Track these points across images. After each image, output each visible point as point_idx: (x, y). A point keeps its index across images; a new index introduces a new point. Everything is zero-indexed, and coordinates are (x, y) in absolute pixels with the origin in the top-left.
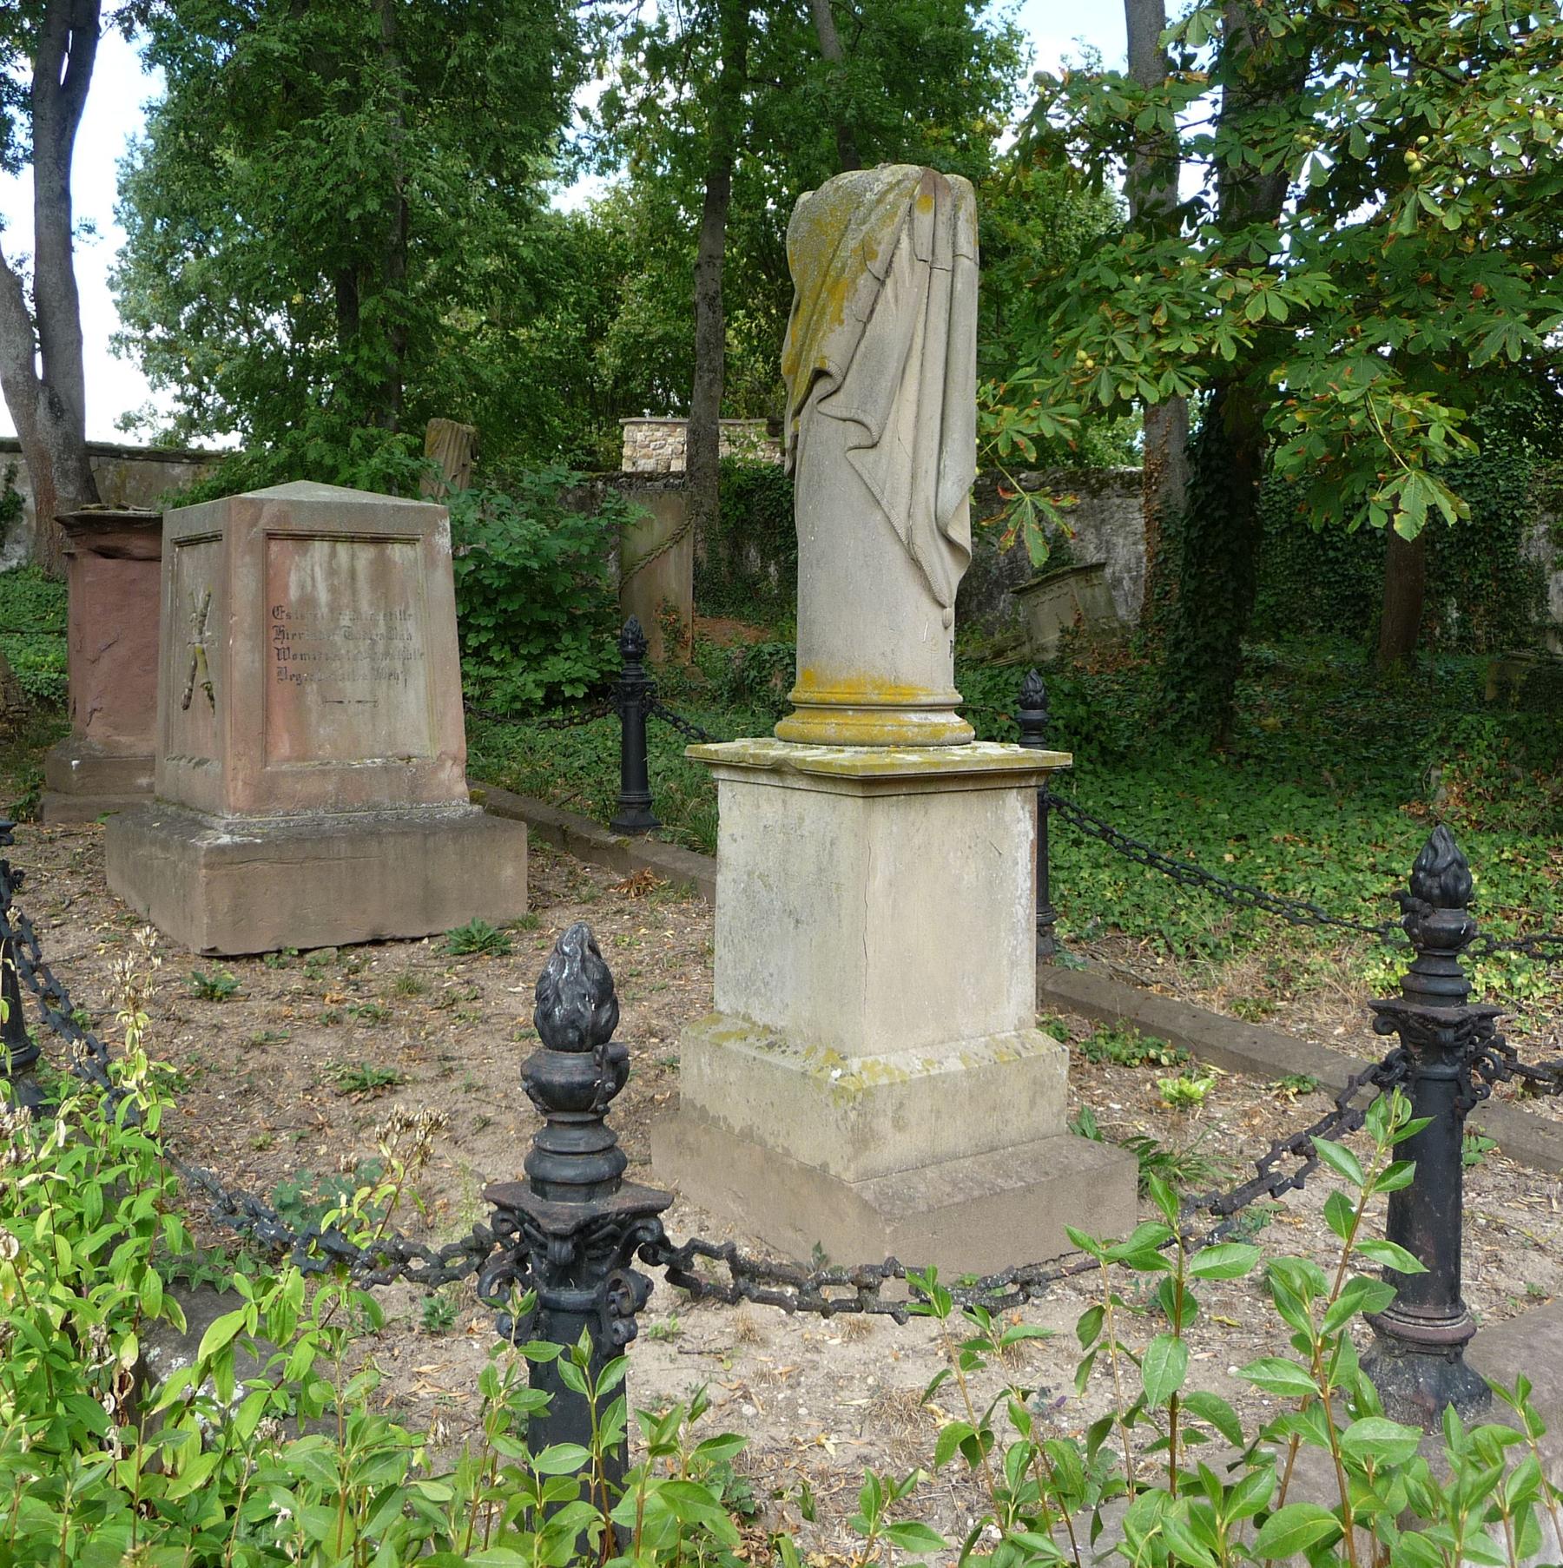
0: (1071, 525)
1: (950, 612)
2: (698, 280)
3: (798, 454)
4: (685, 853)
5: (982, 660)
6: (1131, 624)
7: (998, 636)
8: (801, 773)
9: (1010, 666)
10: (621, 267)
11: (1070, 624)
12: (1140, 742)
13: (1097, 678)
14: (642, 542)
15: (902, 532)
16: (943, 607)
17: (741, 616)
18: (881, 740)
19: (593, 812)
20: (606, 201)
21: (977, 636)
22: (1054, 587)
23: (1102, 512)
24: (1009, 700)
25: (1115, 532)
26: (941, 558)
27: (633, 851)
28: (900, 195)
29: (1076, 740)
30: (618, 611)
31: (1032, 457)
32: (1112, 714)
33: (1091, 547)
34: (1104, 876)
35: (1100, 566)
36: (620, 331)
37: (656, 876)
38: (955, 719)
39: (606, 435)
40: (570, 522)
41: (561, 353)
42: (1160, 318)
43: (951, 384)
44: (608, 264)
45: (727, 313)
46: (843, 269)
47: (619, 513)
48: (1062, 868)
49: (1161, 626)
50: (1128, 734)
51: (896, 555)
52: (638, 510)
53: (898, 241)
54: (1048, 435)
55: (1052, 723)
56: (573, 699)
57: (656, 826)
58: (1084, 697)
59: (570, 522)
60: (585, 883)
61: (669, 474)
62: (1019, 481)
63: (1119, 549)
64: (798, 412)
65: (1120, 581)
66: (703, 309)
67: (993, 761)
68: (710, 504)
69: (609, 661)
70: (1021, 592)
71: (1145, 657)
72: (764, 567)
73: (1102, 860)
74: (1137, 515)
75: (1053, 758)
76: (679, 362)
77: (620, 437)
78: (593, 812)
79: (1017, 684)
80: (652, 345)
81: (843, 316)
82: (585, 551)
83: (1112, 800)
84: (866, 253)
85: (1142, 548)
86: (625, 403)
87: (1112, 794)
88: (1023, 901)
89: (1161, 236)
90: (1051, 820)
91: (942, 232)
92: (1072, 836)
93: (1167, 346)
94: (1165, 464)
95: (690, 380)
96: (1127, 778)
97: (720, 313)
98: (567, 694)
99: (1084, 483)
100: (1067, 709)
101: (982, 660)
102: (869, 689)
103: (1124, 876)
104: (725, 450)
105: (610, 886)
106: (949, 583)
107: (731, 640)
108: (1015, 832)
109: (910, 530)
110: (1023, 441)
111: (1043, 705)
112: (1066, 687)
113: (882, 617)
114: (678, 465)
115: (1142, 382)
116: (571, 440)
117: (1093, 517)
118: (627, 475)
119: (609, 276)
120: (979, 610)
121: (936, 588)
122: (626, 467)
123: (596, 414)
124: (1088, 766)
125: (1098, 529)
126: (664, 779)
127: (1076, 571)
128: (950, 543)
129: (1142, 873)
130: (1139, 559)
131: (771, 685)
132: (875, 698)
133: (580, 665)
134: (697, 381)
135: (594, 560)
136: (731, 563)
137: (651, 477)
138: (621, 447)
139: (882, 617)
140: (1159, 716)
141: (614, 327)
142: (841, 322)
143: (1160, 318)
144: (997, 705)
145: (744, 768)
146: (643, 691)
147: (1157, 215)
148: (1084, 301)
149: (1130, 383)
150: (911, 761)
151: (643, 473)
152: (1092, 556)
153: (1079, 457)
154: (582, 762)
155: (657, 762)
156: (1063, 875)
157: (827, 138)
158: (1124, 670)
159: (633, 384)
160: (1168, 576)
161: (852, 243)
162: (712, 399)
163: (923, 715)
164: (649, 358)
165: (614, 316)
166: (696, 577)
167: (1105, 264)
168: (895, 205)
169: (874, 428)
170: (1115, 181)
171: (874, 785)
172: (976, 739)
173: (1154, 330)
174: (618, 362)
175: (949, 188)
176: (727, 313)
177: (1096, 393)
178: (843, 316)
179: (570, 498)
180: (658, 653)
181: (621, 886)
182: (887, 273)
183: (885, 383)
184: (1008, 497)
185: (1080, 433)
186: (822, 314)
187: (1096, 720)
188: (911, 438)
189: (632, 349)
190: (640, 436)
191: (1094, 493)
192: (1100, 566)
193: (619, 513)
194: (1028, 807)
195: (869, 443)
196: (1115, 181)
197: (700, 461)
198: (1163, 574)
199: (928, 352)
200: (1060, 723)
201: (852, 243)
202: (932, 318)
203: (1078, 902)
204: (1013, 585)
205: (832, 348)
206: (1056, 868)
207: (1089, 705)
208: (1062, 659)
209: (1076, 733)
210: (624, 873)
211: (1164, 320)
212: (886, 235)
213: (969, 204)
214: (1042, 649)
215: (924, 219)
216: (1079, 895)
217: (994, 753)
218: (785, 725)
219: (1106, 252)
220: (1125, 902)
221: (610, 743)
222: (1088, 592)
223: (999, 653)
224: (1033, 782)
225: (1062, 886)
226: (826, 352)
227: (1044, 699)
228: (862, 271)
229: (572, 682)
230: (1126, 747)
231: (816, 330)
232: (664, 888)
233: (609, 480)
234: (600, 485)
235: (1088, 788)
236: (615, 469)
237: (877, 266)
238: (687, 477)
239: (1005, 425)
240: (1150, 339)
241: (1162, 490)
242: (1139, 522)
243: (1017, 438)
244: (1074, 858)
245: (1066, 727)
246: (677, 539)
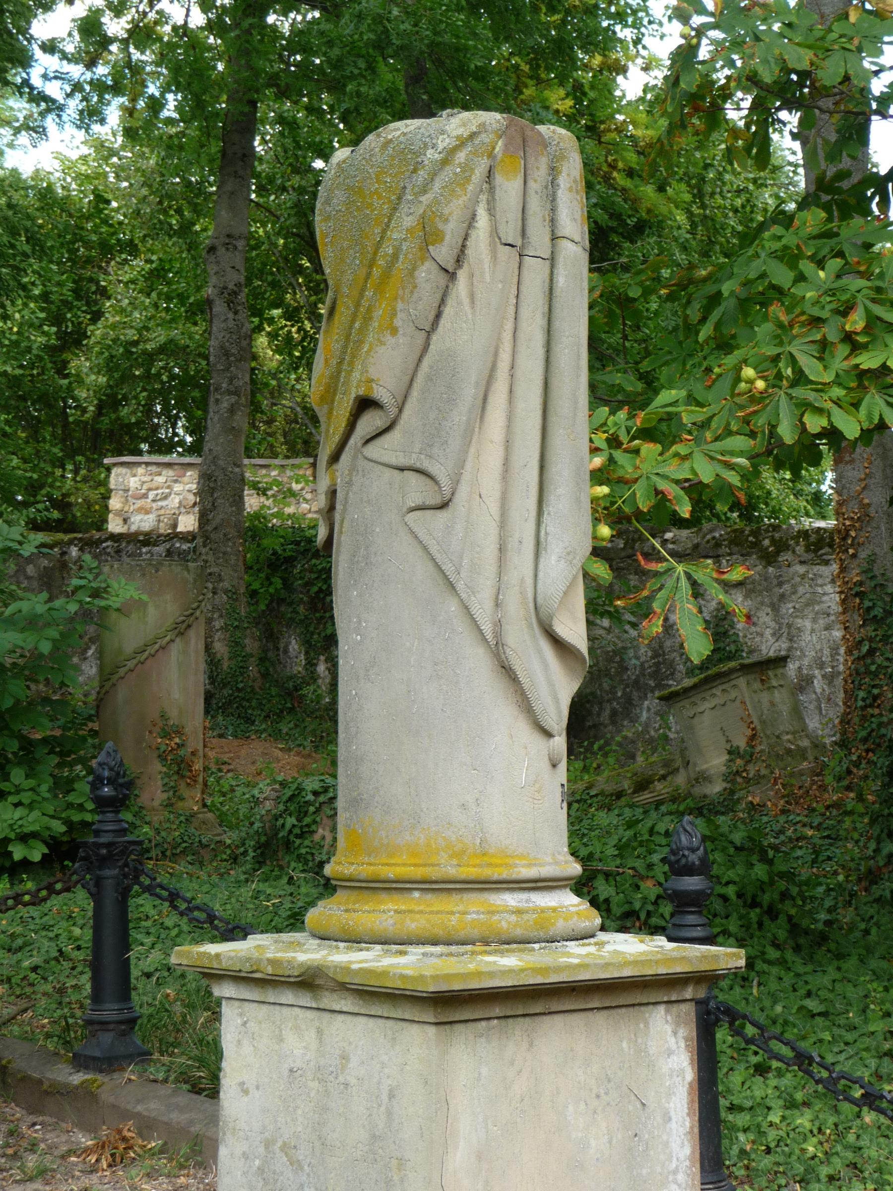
0: (738, 603)
1: (560, 742)
2: (212, 269)
3: (337, 517)
4: (185, 1098)
5: (619, 795)
6: (827, 741)
7: (640, 759)
8: (343, 987)
9: (658, 804)
10: (106, 249)
11: (741, 743)
12: (847, 916)
13: (782, 819)
14: (129, 634)
15: (487, 628)
16: (548, 734)
17: (277, 735)
18: (462, 934)
19: (48, 1036)
20: (84, 158)
21: (611, 760)
22: (717, 691)
23: (780, 584)
24: (656, 858)
25: (799, 612)
26: (546, 666)
27: (106, 1096)
28: (475, 153)
29: (754, 914)
30: (94, 733)
31: (685, 510)
32: (805, 873)
33: (768, 632)
34: (803, 1121)
35: (780, 661)
36: (104, 336)
37: (140, 1135)
38: (569, 900)
39: (85, 480)
40: (25, 606)
41: (21, 366)
42: (856, 322)
43: (552, 419)
44: (88, 245)
45: (257, 312)
46: (395, 256)
47: (96, 594)
48: (741, 1109)
49: (870, 745)
50: (828, 903)
51: (477, 663)
52: (123, 588)
53: (473, 217)
54: (706, 481)
55: (719, 890)
56: (25, 864)
57: (142, 1056)
58: (763, 853)
59: (25, 606)
60: (33, 1147)
61: (175, 536)
62: (664, 542)
63: (806, 637)
64: (335, 458)
65: (809, 680)
66: (219, 307)
67: (627, 963)
68: (232, 578)
69: (81, 807)
70: (670, 698)
71: (848, 788)
72: (311, 664)
73: (799, 1096)
74: (829, 588)
75: (716, 957)
76: (187, 381)
77: (105, 483)
78: (48, 1036)
79: (667, 834)
80: (150, 357)
81: (398, 322)
82: (45, 648)
83: (812, 1005)
84: (428, 234)
85: (838, 634)
86: (118, 435)
87: (809, 994)
88: (681, 1177)
89: (846, 214)
90: (722, 1035)
91: (536, 205)
92: (754, 1060)
93: (868, 361)
94: (865, 518)
95: (203, 404)
96: (831, 969)
97: (243, 314)
98: (17, 856)
99: (754, 545)
100: (740, 869)
101: (619, 795)
102: (443, 858)
103: (831, 1120)
104: (252, 502)
105: (70, 1153)
106: (556, 700)
107: (259, 770)
108: (665, 1070)
109: (498, 624)
110: (673, 490)
111: (703, 868)
112: (738, 837)
113: (461, 751)
114: (188, 523)
115: (835, 410)
116: (33, 488)
117: (769, 592)
118: (116, 538)
119: (89, 261)
120: (613, 722)
121: (538, 708)
122: (114, 526)
123: (71, 453)
124: (773, 954)
125: (775, 608)
126: (158, 984)
127: (746, 669)
128: (557, 642)
129: (858, 1116)
130: (835, 650)
131: (317, 837)
132: (452, 871)
133: (36, 814)
134: (212, 407)
135: (60, 654)
136: (262, 660)
137: (147, 539)
138: (106, 497)
139: (461, 751)
140: (872, 877)
141: (97, 332)
142: (394, 331)
143: (856, 322)
144: (639, 864)
145: (261, 981)
146: (125, 852)
147: (839, 191)
148: (744, 304)
149: (820, 411)
150: (507, 966)
151: (137, 533)
152: (770, 647)
153: (747, 510)
154: (36, 960)
155: (144, 958)
156: (742, 1119)
157: (391, 74)
158: (820, 808)
159: (124, 411)
160: (875, 674)
161: (407, 220)
162: (234, 431)
163: (524, 896)
164: (147, 376)
165: (97, 316)
166: (212, 679)
167: (773, 254)
168: (467, 168)
169: (444, 481)
170: (786, 146)
171: (452, 1006)
172: (603, 928)
173: (848, 338)
174: (102, 380)
175: (544, 143)
176: (257, 312)
177: (773, 427)
178: (398, 322)
179: (30, 570)
180: (153, 793)
181: (87, 1151)
182: (459, 261)
183: (460, 416)
184: (654, 566)
185: (750, 476)
186: (368, 319)
187: (782, 885)
188: (497, 494)
189: (125, 363)
190: (133, 483)
191: (769, 559)
192: (780, 661)
193: (96, 594)
194: (682, 1032)
195: (437, 501)
196: (786, 146)
197: (217, 518)
198: (868, 672)
199: (519, 373)
200: (731, 891)
201: (407, 220)
202: (523, 324)
203: (767, 1162)
204: (659, 686)
205: (382, 366)
206: (732, 1108)
207: (770, 862)
208: (732, 792)
209: (754, 904)
210: (90, 1129)
211: (860, 325)
212: (455, 209)
213: (572, 169)
214: (703, 778)
215: (509, 188)
216: (768, 1151)
217: (630, 951)
218: (323, 913)
219: (769, 241)
220: (835, 1160)
221: (77, 931)
222: (765, 697)
223: (642, 785)
224: (689, 993)
225: (742, 1137)
226: (373, 373)
227: (704, 860)
228: (423, 260)
229: (24, 838)
230: (828, 923)
231: (360, 343)
232: (152, 1153)
233: (87, 545)
234: (74, 551)
235: (773, 986)
236: (99, 529)
237: (444, 253)
238: (199, 541)
239: (645, 468)
240: (843, 350)
241: (863, 554)
242: (831, 598)
243: (663, 485)
244: (758, 1093)
245: (740, 895)
246: (181, 629)
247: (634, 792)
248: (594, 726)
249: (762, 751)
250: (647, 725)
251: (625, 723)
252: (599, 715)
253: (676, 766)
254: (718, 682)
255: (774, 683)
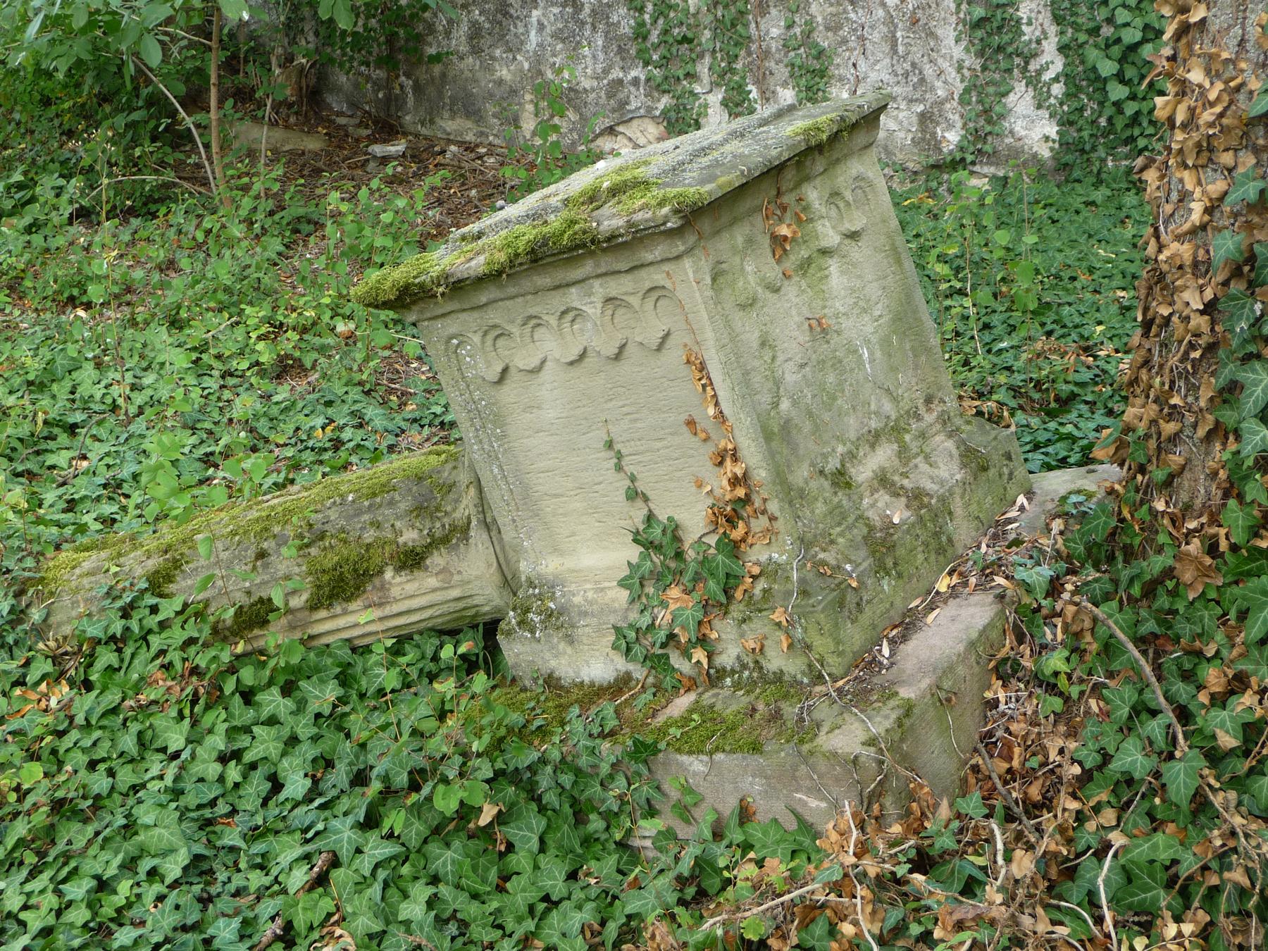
22: (589, 299)
120: (476, 51)
222: (789, 311)
247: (314, 606)
248: (437, 58)
249: (770, 571)
250: (538, 60)
251: (498, 52)
252: (448, 33)
253: (460, 514)
254: (588, 267)
255: (829, 234)
